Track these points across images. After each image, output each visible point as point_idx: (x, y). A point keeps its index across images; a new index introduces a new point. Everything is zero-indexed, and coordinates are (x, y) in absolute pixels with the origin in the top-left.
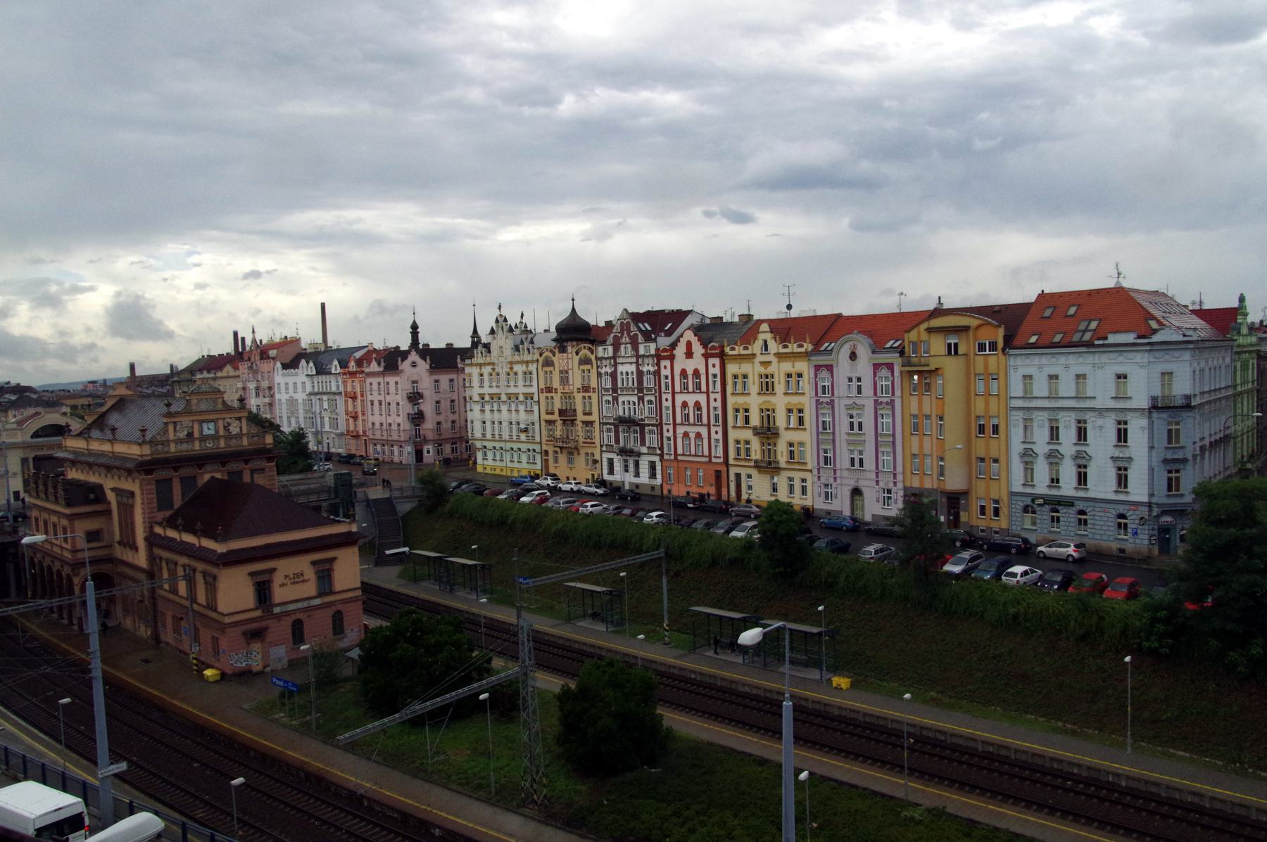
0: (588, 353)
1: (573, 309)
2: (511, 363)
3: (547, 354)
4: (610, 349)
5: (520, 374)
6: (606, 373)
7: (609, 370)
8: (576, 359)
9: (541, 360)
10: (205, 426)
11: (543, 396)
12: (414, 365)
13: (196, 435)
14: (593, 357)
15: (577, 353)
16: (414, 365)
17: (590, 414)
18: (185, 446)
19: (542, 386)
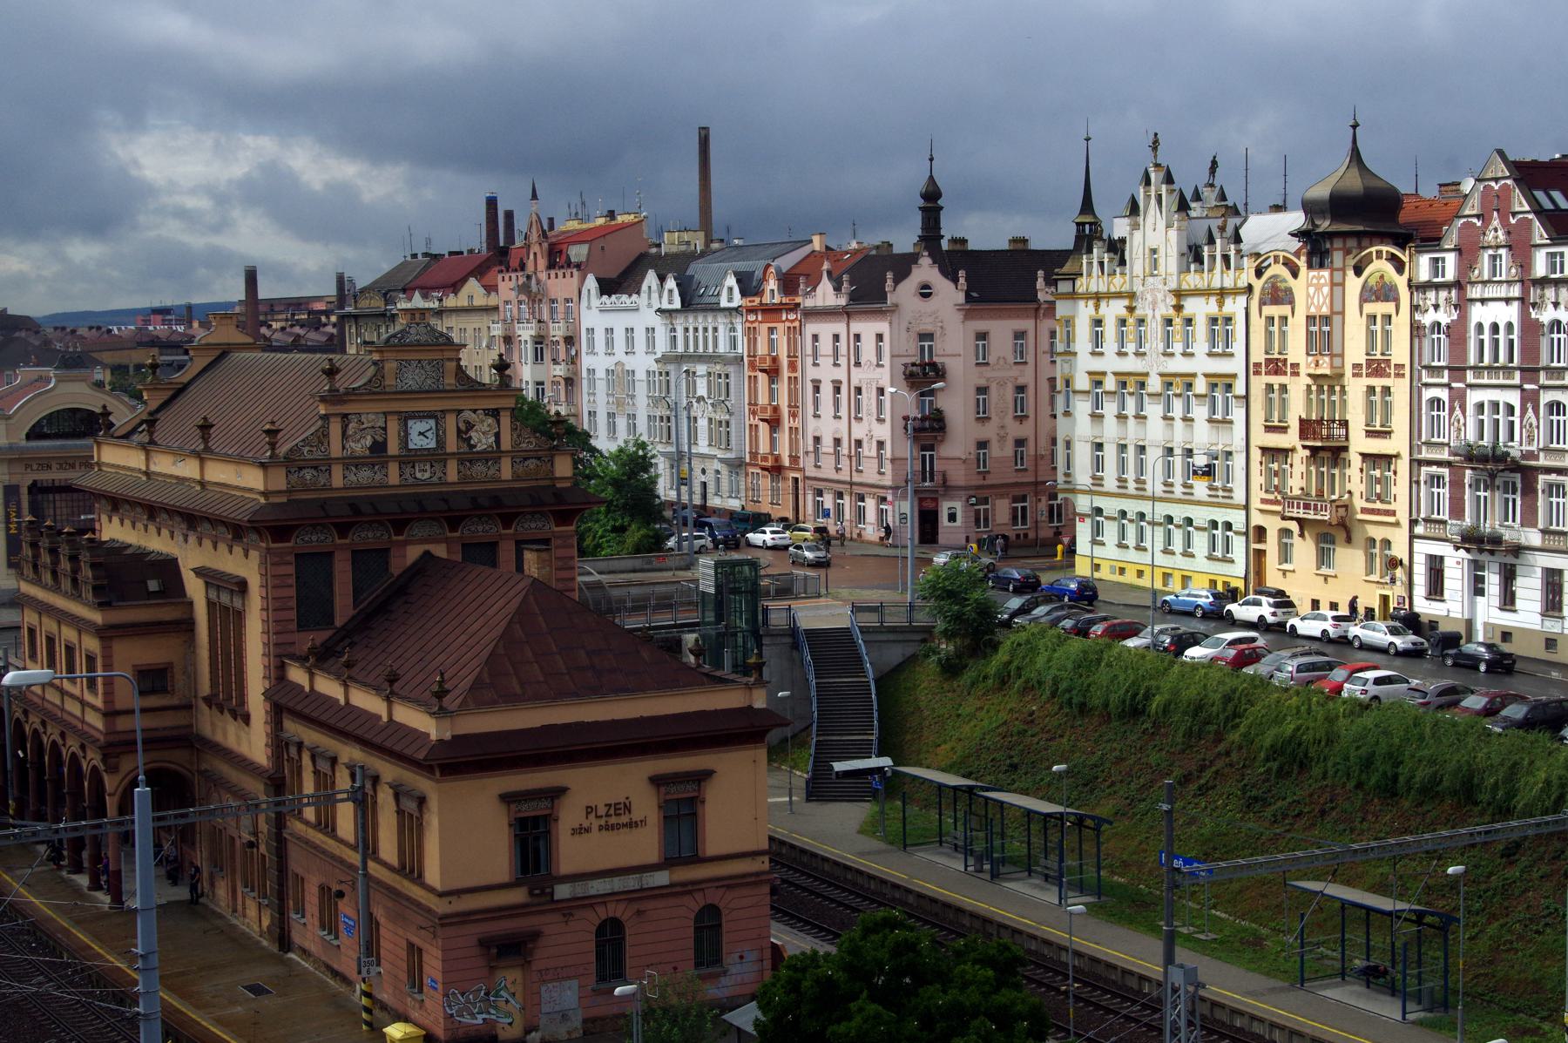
9: (1258, 285)
10: (416, 427)
12: (925, 292)
13: (393, 448)
16: (925, 292)
17: (1385, 434)
18: (364, 475)
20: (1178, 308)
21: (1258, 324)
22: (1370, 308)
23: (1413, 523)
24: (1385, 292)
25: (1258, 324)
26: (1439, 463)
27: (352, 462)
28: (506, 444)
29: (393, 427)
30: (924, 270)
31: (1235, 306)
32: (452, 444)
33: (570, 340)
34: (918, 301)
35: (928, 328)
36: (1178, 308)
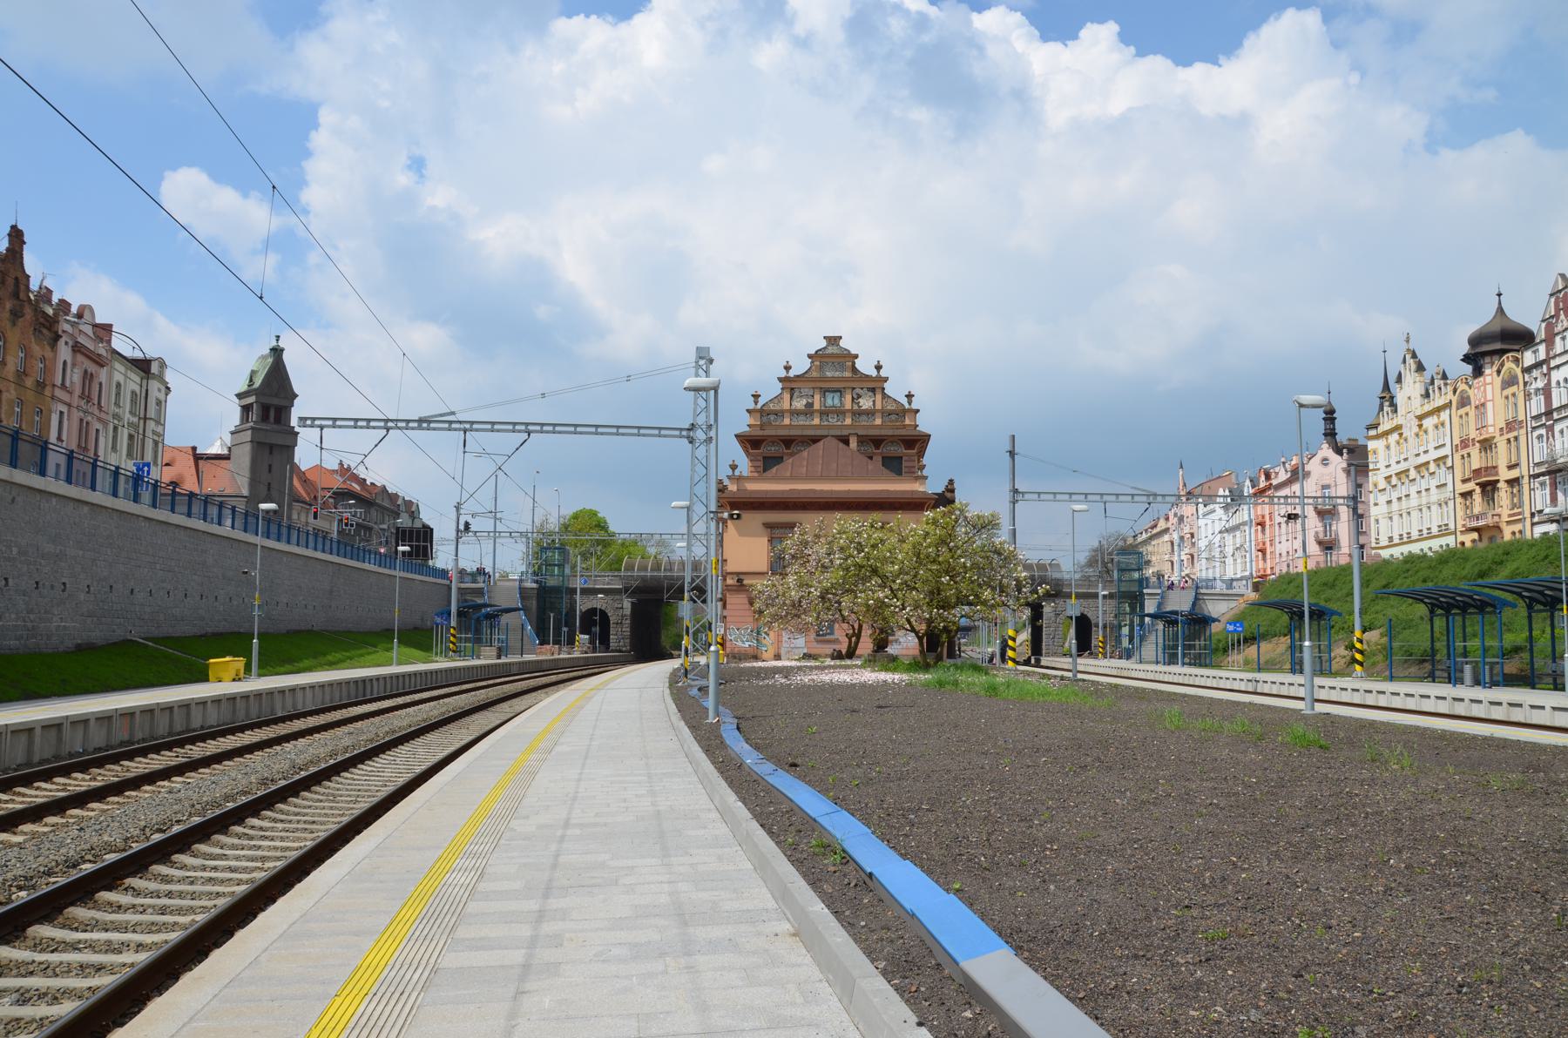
0: (1513, 366)
1: (1500, 310)
2: (1421, 418)
3: (1462, 387)
4: (1542, 348)
5: (1431, 429)
6: (1537, 390)
7: (1540, 384)
8: (1498, 381)
9: (1455, 400)
10: (829, 396)
11: (1457, 457)
12: (1325, 462)
13: (817, 406)
14: (1518, 371)
15: (1499, 372)
16: (1325, 462)
17: (1516, 466)
18: (802, 421)
19: (1457, 441)
20: (1420, 426)
21: (1455, 420)
22: (1506, 392)
23: (1533, 515)
24: (1510, 382)
25: (1455, 420)
26: (1543, 474)
27: (795, 413)
28: (879, 407)
29: (817, 397)
30: (1326, 451)
31: (1445, 415)
32: (848, 406)
33: (1192, 535)
34: (1321, 468)
35: (1326, 482)
36: (1420, 426)
